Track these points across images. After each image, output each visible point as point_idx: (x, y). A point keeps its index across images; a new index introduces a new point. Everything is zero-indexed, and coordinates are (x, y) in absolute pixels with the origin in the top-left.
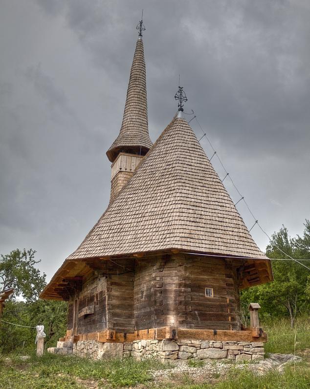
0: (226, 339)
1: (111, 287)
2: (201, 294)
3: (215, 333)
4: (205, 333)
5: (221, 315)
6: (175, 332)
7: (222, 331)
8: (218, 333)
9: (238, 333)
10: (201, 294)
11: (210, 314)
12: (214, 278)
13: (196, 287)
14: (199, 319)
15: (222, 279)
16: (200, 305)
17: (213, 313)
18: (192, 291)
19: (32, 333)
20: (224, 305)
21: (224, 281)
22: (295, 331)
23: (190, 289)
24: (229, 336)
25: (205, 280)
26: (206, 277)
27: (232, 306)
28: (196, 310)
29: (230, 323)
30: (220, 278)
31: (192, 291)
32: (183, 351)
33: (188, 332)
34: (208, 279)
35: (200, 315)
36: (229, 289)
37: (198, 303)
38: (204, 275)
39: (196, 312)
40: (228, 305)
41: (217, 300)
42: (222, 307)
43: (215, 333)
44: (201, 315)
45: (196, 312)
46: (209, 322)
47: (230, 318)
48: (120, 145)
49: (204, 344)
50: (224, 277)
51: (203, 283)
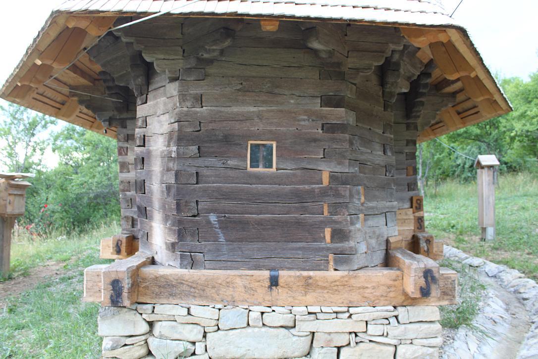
0: (310, 298)
1: (126, 145)
2: (231, 163)
3: (274, 282)
4: (239, 282)
5: (299, 224)
6: (121, 288)
7: (298, 273)
8: (281, 281)
9: (353, 281)
10: (231, 163)
11: (260, 223)
12: (281, 111)
13: (217, 141)
14: (222, 239)
15: (306, 112)
16: (227, 196)
17: (273, 219)
18: (201, 153)
19: (27, 218)
20: (312, 191)
21: (313, 115)
22: (524, 183)
23: (194, 149)
24: (324, 288)
25: (247, 118)
26: (252, 109)
27: (337, 194)
28: (214, 211)
29: (328, 249)
30: (302, 109)
31: (201, 153)
32: (161, 337)
33: (181, 282)
34: (260, 116)
35: (225, 225)
36: (333, 140)
37: (218, 190)
38: (244, 103)
39: (213, 218)
40: (324, 193)
41: (288, 176)
42: (300, 198)
43: (274, 282)
44: (225, 225)
45: (213, 218)
46: (256, 245)
47: (328, 232)
48: (402, 67)
49: (232, 316)
50: (316, 105)
51: (239, 128)
